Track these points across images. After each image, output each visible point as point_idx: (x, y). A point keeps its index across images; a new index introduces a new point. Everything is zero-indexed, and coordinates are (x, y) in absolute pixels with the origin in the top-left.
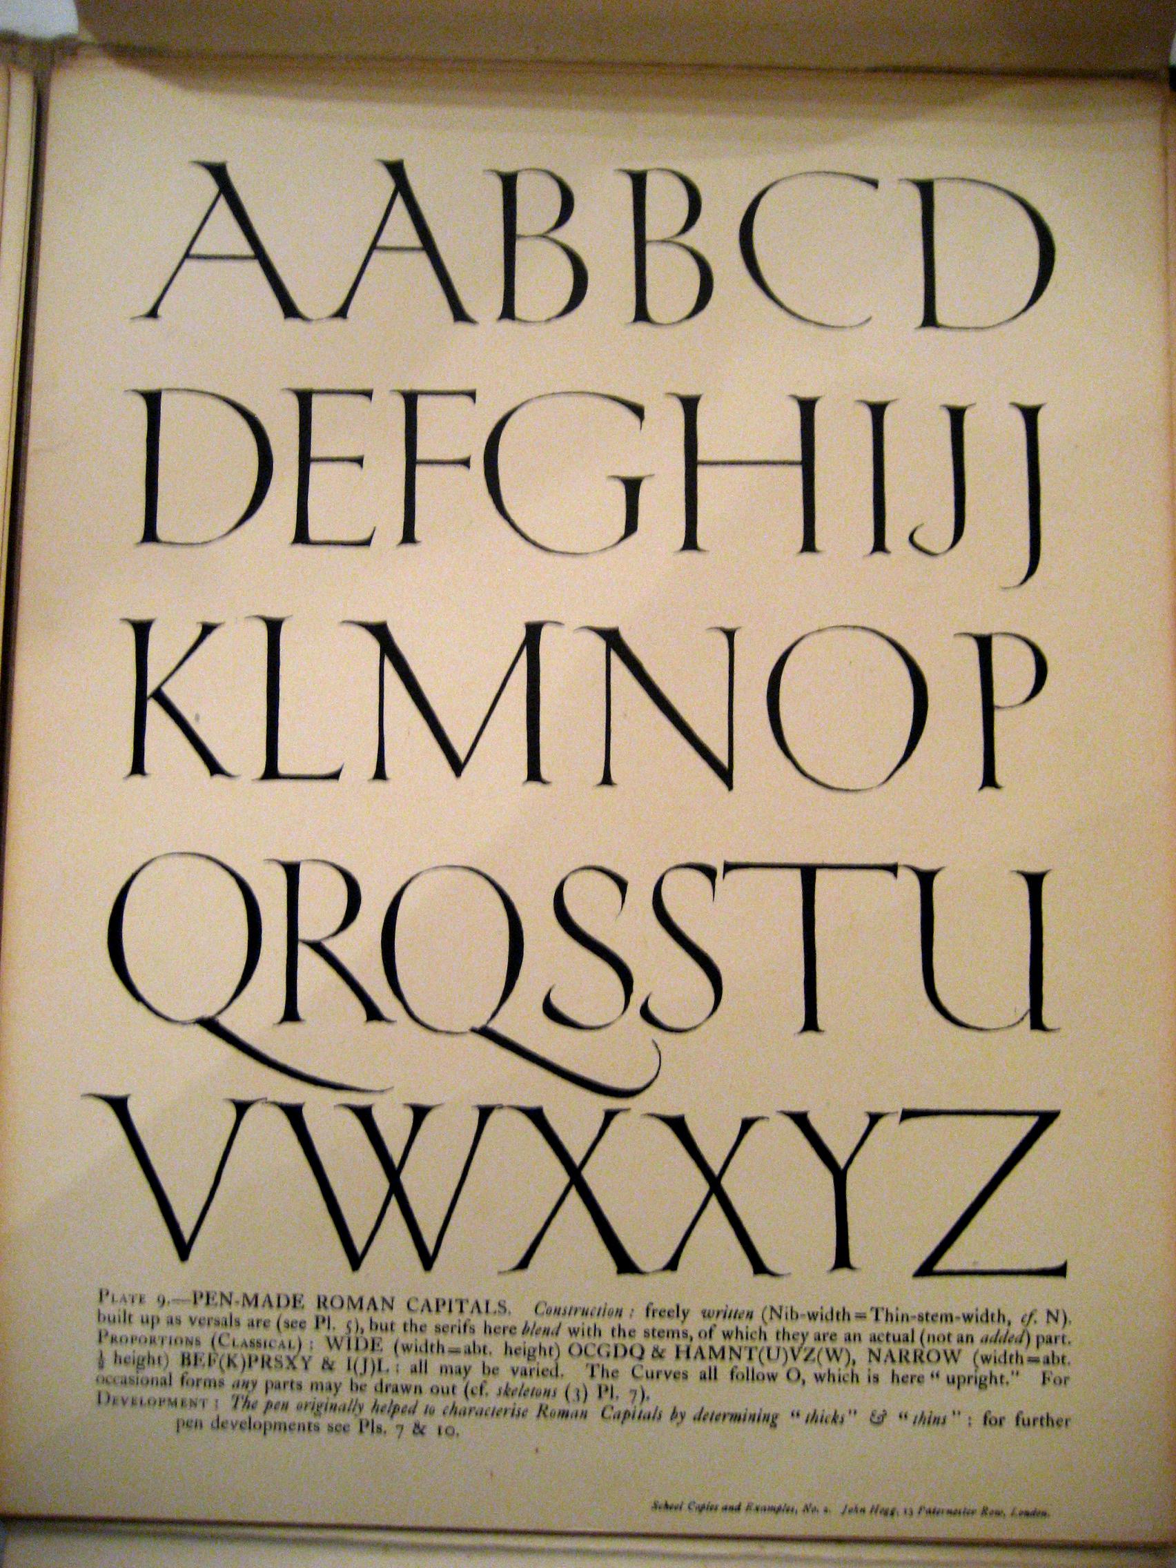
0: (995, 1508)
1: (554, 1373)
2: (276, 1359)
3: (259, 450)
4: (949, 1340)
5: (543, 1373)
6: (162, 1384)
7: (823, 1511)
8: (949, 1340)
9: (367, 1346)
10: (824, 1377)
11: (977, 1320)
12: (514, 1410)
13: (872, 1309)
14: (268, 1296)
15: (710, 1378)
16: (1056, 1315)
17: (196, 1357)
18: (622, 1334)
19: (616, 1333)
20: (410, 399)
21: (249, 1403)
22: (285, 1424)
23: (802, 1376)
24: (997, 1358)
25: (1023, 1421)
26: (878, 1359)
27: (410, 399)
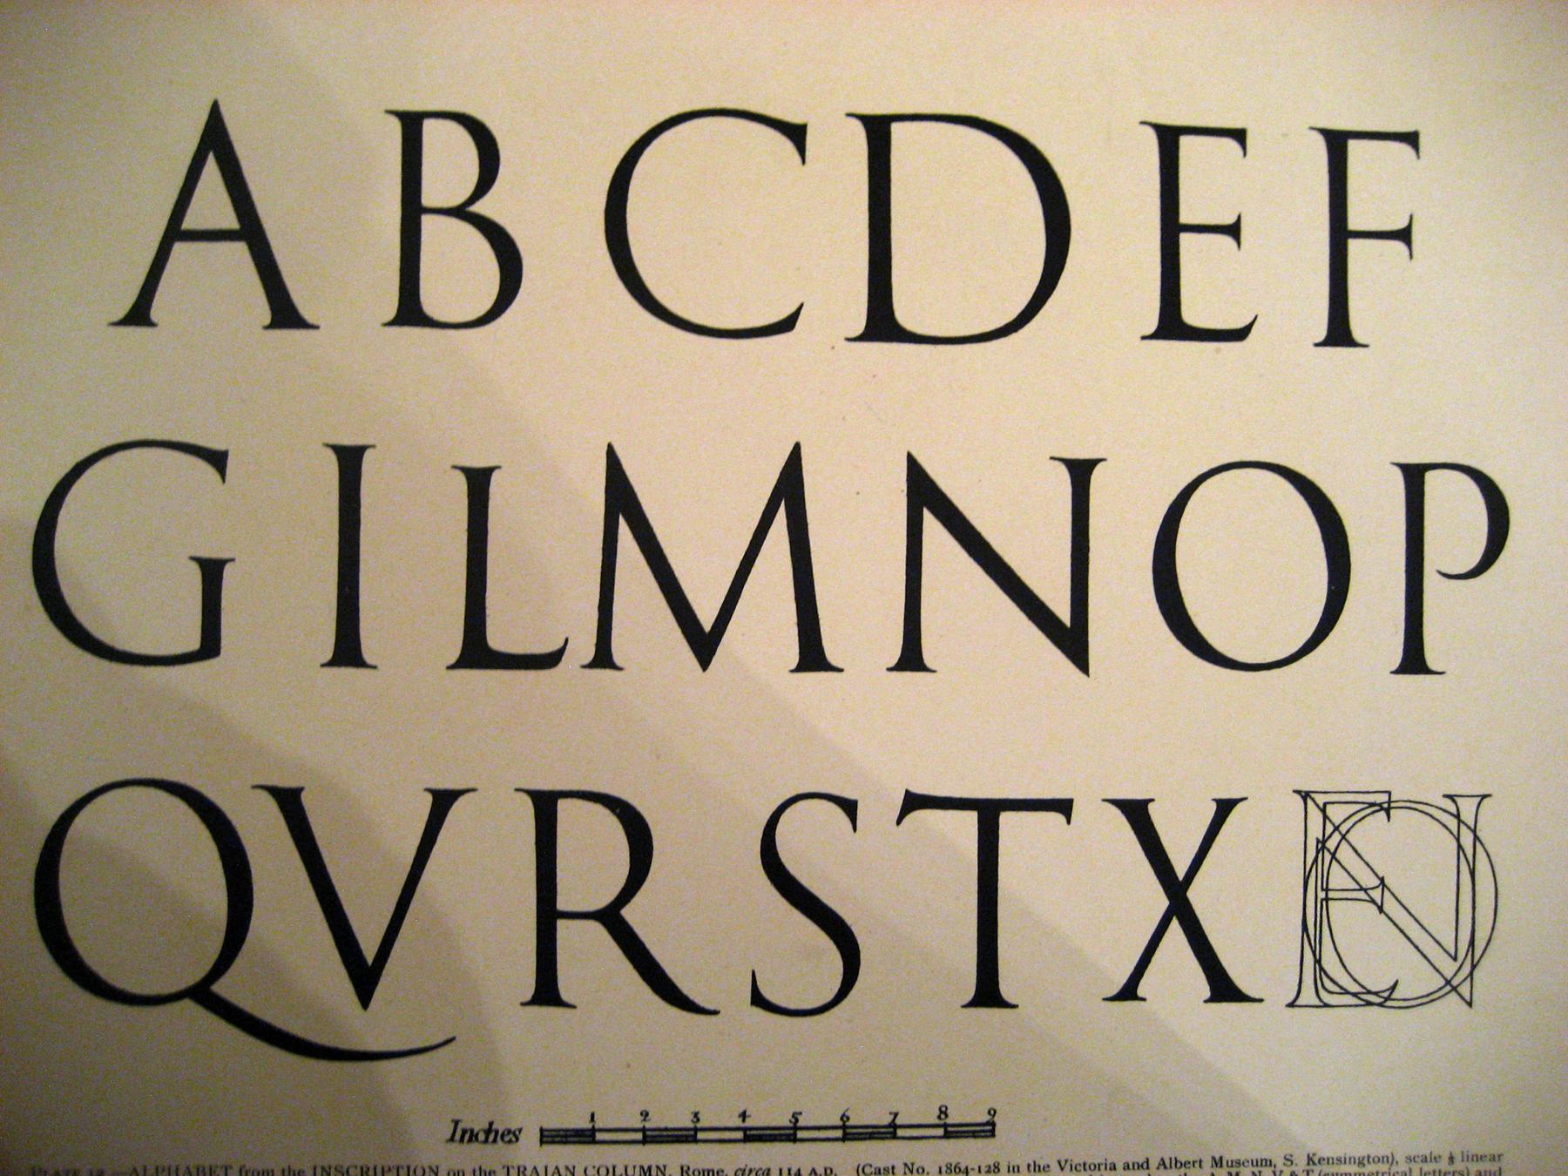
0: (1235, 1157)
1: (1145, 1166)
2: (336, 1168)
3: (1174, 552)
4: (893, 1173)
5: (1076, 1168)
6: (1110, 1169)
7: (497, 1171)
8: (893, 1173)
9: (415, 1170)
10: (554, 1173)
11: (1071, 1169)
12: (745, 1170)
13: (504, 1167)
14: (557, 1168)
15: (1171, 1166)
16: (572, 1170)
17: (211, 1170)
18: (1037, 1168)
19: (1032, 1168)
20: (878, 130)
21: (294, 1172)
22: (1354, 1158)
23: (834, 1172)
24: (1074, 1166)
25: (1227, 1162)
26: (912, 1172)
27: (878, 130)
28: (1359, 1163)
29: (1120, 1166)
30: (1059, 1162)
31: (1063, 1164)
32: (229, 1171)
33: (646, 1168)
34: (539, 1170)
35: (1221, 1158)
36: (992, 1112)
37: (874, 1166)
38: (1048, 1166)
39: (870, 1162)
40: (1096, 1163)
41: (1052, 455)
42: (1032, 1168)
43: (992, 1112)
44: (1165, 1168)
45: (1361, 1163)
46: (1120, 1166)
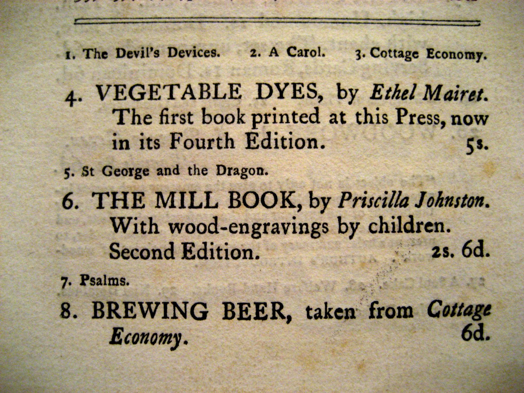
19: (192, 172)
28: (313, 232)
29: (421, 311)
30: (99, 87)
31: (104, 89)
32: (220, 141)
33: (433, 89)
34: (181, 316)
35: (439, 87)
36: (257, 83)
37: (298, 49)
38: (148, 170)
39: (294, 45)
40: (241, 249)
41: (352, 206)
42: (192, 172)
43: (257, 83)
44: (193, 98)
45: (244, 177)
46: (421, 311)
